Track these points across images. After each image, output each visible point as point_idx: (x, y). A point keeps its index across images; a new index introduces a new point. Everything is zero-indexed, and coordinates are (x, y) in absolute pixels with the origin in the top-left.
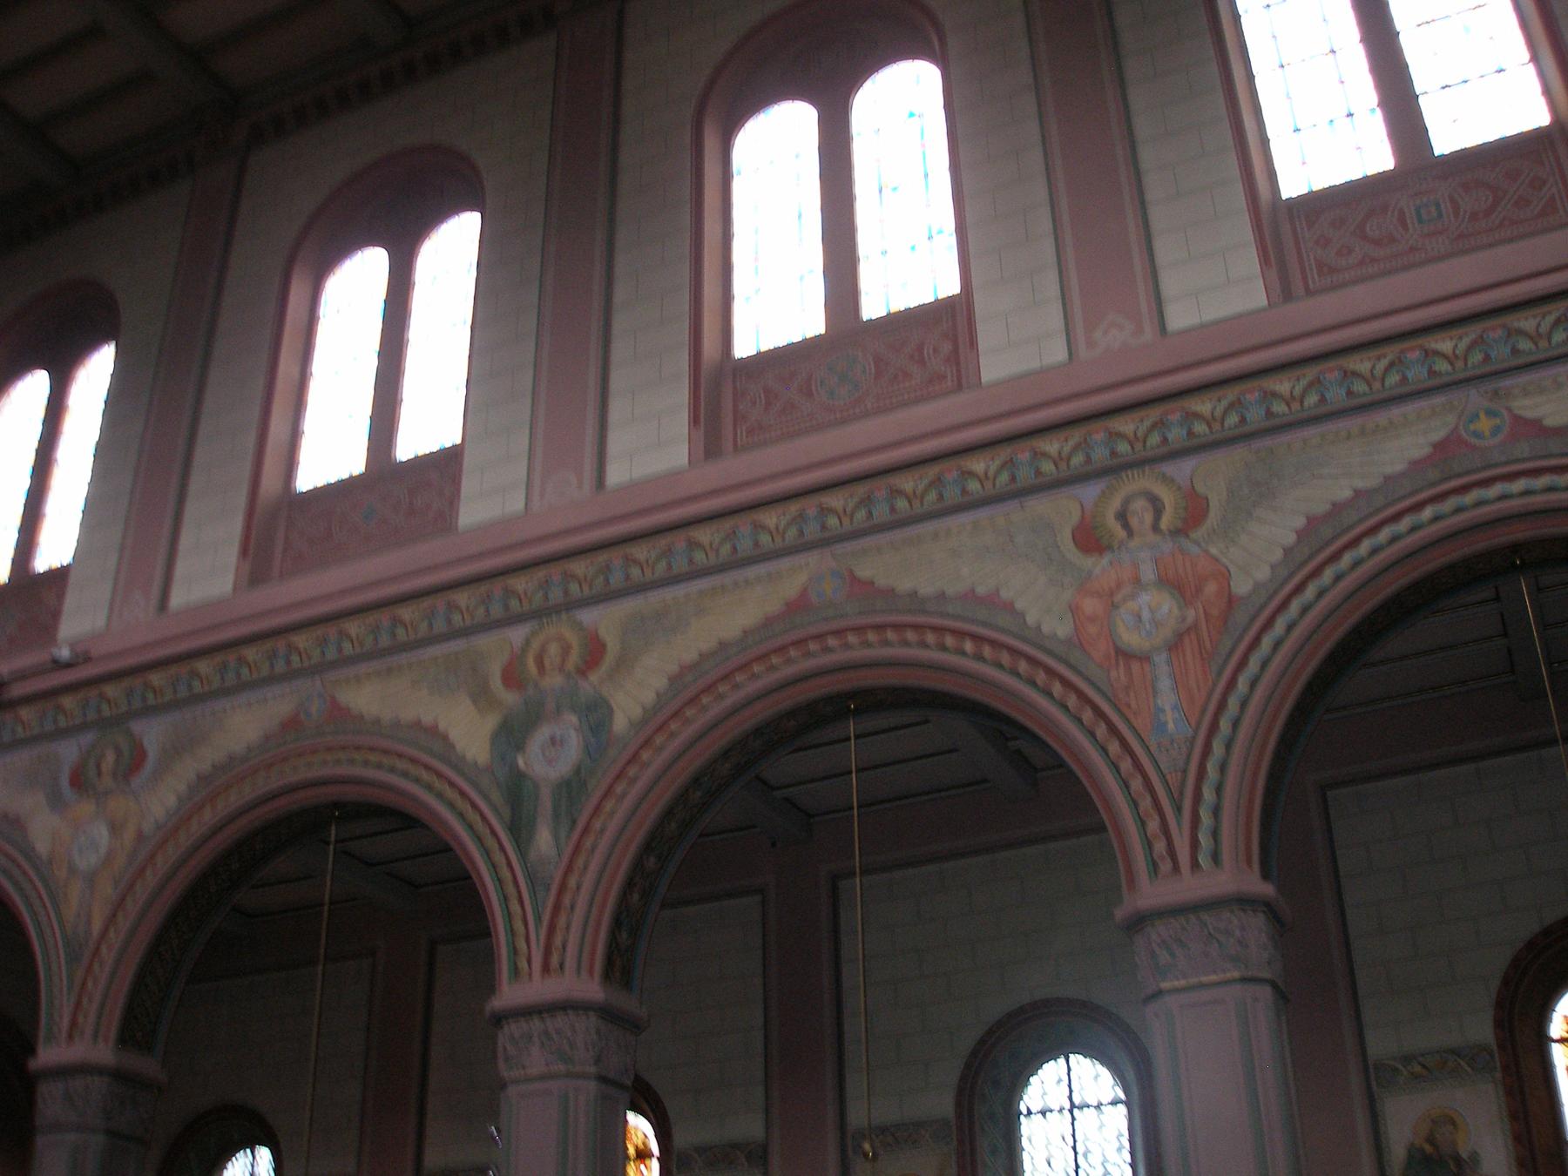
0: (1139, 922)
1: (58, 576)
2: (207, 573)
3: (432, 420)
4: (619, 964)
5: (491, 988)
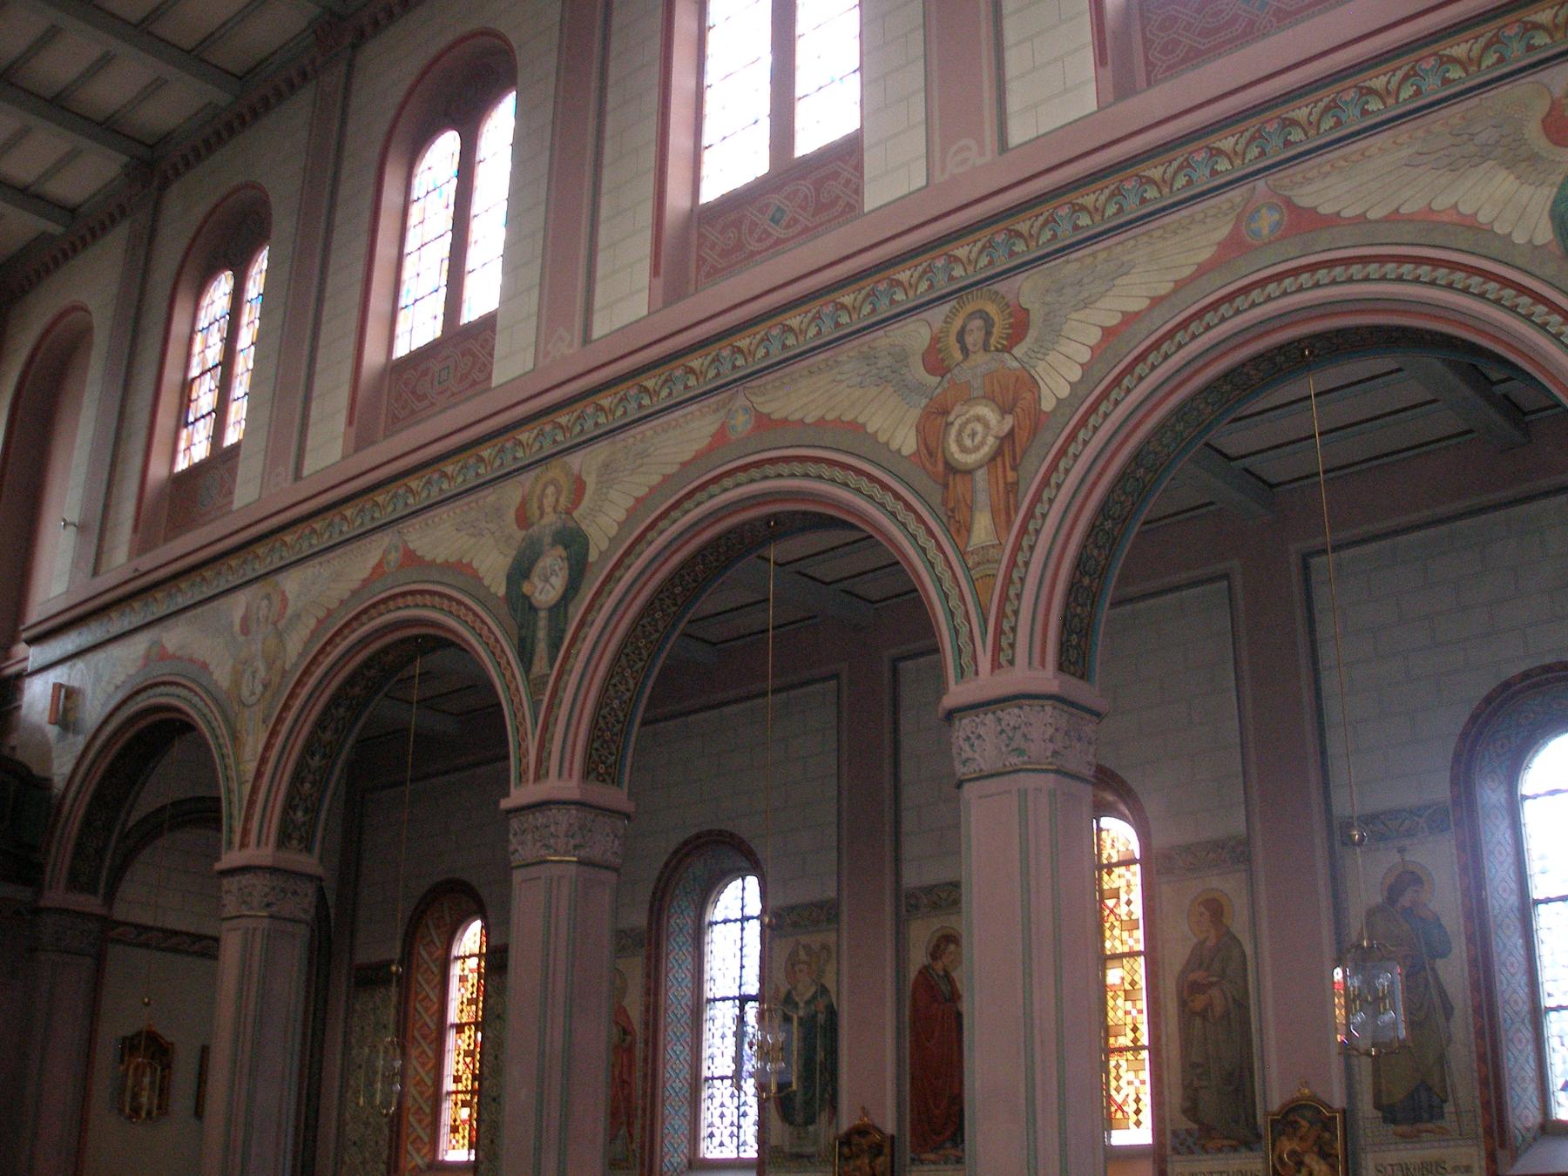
0: (950, 715)
1: (236, 447)
2: (626, 300)
3: (829, 114)
4: (1074, 654)
5: (942, 689)
